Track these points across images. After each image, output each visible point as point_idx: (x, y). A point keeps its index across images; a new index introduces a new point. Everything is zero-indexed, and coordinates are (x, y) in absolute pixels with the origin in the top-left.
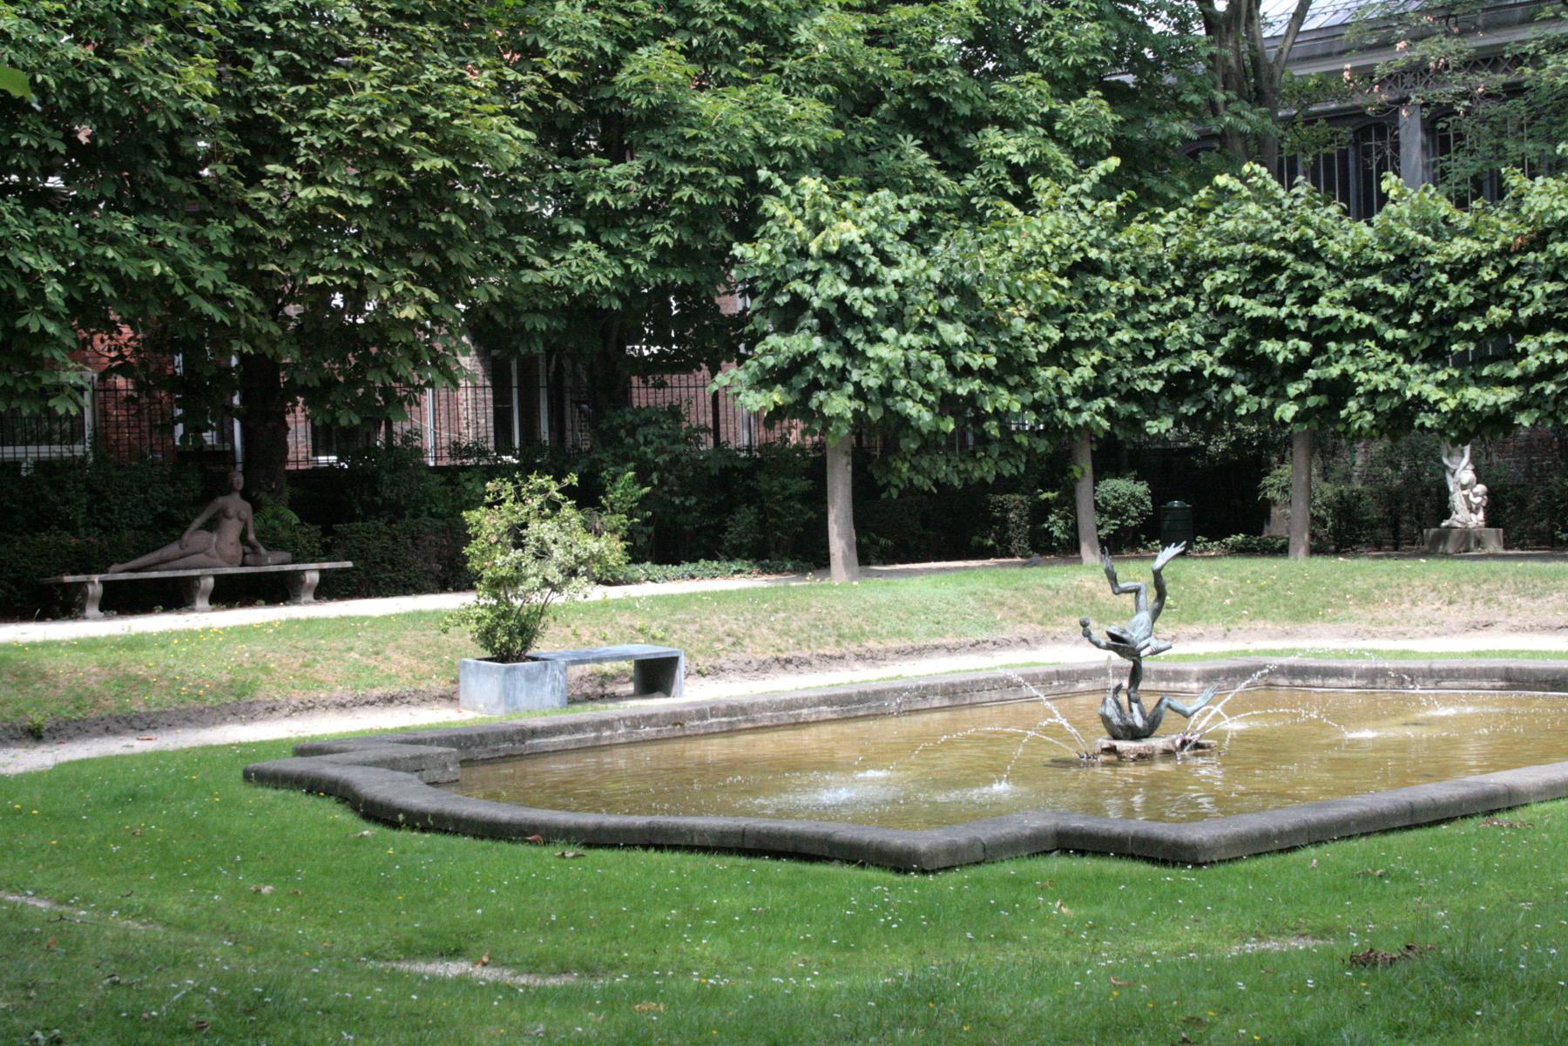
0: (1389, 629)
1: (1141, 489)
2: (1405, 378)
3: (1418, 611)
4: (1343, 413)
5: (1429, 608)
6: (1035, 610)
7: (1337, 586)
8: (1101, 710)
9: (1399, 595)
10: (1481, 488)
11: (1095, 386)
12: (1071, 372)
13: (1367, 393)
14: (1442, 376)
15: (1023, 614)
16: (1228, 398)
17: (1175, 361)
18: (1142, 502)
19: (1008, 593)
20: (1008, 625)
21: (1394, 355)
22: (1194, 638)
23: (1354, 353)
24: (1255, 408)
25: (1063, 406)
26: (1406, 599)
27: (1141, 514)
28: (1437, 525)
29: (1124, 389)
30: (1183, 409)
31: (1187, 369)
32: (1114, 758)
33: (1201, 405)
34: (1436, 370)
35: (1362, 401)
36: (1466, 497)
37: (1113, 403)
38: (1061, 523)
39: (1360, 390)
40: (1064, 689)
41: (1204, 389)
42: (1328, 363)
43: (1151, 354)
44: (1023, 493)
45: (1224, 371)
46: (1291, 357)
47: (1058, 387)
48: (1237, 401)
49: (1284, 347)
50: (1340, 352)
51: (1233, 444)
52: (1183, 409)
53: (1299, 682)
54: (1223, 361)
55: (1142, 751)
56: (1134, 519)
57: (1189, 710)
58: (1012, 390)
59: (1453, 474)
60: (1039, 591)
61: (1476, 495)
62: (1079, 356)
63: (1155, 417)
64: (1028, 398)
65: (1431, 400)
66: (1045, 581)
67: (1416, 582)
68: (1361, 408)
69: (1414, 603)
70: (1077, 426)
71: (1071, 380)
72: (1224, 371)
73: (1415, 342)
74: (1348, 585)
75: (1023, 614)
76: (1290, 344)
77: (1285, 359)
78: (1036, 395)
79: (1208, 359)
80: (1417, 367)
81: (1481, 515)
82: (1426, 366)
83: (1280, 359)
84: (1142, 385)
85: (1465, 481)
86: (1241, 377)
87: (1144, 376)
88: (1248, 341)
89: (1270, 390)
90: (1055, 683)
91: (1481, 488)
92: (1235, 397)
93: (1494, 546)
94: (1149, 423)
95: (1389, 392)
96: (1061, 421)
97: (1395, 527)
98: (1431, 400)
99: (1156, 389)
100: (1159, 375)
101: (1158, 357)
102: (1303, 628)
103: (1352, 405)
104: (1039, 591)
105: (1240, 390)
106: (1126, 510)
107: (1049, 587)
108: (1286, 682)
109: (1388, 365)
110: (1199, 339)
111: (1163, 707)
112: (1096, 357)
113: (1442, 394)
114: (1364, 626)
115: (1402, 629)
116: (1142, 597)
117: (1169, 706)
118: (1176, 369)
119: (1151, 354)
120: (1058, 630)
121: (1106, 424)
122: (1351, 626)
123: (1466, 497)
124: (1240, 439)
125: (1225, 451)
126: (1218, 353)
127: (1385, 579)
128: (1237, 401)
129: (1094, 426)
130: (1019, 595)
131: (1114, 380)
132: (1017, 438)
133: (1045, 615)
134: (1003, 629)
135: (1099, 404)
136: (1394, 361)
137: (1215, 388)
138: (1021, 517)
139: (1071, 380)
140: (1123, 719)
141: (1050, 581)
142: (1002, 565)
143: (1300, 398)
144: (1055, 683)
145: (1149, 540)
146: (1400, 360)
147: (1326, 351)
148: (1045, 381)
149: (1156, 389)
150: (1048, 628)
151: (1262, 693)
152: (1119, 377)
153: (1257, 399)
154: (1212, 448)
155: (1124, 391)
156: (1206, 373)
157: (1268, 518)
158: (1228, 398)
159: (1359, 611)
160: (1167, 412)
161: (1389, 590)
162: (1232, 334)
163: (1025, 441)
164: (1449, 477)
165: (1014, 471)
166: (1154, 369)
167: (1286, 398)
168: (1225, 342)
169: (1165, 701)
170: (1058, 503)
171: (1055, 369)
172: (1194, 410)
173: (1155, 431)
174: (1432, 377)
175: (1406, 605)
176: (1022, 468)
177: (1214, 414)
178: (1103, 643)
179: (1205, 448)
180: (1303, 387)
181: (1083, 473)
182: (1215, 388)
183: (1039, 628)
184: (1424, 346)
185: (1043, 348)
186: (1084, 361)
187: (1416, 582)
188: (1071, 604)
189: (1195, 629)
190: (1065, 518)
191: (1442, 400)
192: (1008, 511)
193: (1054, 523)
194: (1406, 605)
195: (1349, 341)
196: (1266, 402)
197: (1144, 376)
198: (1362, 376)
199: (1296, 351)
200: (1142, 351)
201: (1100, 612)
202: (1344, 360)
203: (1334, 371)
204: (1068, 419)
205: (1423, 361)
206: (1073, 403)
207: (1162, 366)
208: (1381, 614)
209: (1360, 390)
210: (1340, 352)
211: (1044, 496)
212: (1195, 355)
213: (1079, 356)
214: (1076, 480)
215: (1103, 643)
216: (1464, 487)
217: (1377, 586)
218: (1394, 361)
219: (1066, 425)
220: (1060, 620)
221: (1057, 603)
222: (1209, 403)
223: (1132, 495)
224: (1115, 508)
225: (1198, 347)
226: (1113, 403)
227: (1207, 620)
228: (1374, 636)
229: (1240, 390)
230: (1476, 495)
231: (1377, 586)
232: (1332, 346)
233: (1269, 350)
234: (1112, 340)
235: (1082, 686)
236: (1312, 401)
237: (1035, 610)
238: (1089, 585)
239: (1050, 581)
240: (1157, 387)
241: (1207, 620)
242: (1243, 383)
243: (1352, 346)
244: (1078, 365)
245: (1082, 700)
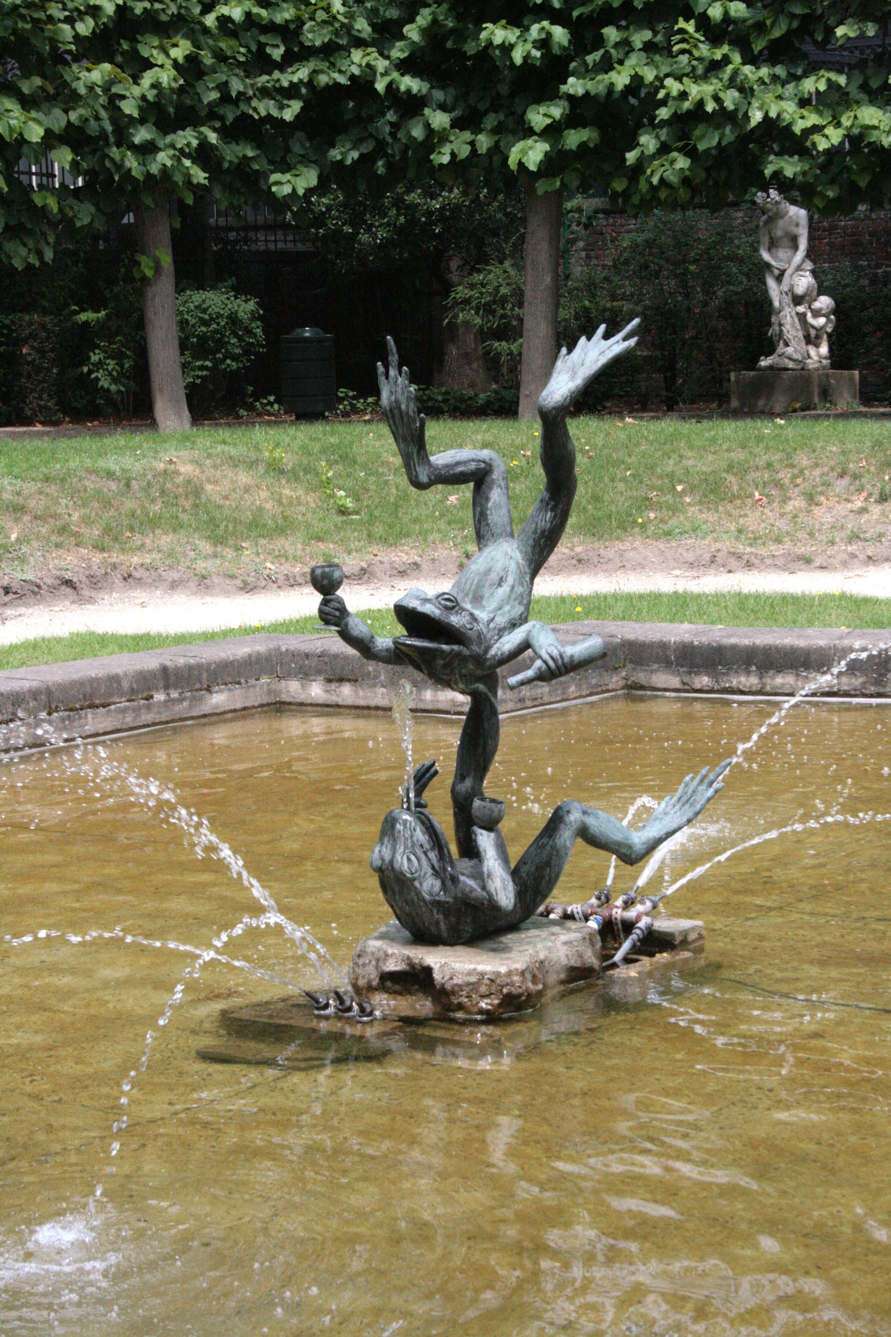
0: (778, 550)
1: (246, 307)
2: (746, 91)
3: (824, 515)
4: (631, 157)
5: (843, 509)
6: (86, 521)
7: (652, 468)
8: (380, 852)
9: (778, 484)
10: (824, 302)
11: (179, 107)
12: (136, 79)
13: (677, 119)
14: (811, 85)
15: (63, 530)
16: (418, 132)
17: (324, 65)
18: (249, 332)
19: (30, 487)
20: (33, 551)
21: (726, 49)
22: (402, 574)
23: (649, 47)
24: (464, 152)
25: (122, 139)
26: (793, 492)
27: (247, 352)
28: (752, 364)
29: (230, 114)
30: (335, 154)
31: (342, 80)
32: (423, 1006)
33: (368, 147)
34: (798, 79)
35: (664, 133)
36: (802, 317)
37: (213, 137)
38: (111, 364)
39: (663, 113)
40: (181, 709)
41: (371, 119)
42: (606, 65)
43: (277, 53)
44: (45, 312)
45: (410, 83)
46: (537, 54)
47: (114, 100)
48: (434, 139)
49: (522, 38)
50: (625, 45)
51: (400, 230)
52: (335, 154)
53: (705, 681)
54: (405, 66)
55: (518, 985)
56: (234, 358)
57: (639, 839)
58: (28, 103)
59: (779, 279)
60: (90, 484)
61: (816, 314)
62: (149, 48)
63: (286, 168)
64: (58, 119)
65: (797, 129)
66: (101, 463)
67: (803, 460)
68: (664, 149)
69: (810, 498)
70: (149, 176)
71: (136, 91)
72: (410, 83)
73: (760, 27)
74: (670, 465)
75: (63, 530)
76: (535, 31)
77: (526, 58)
78: (73, 116)
79: (381, 65)
80: (764, 72)
81: (824, 349)
82: (780, 70)
83: (518, 57)
84: (264, 107)
85: (800, 290)
86: (439, 95)
87: (265, 93)
88: (452, 31)
89: (490, 121)
90: (159, 697)
91: (824, 302)
92: (429, 130)
93: (846, 400)
94: (274, 177)
95: (723, 116)
96: (119, 167)
97: (669, 370)
98: (797, 129)
99: (288, 115)
100: (292, 92)
101: (290, 59)
102: (611, 550)
103: (648, 142)
104: (90, 484)
105: (439, 119)
106: (221, 344)
107: (110, 474)
108: (674, 681)
109: (715, 67)
110: (362, 26)
111: (566, 836)
112: (181, 50)
113: (813, 119)
114: (726, 545)
115: (802, 550)
116: (496, 496)
117: (585, 834)
118: (323, 79)
119: (277, 53)
120: (135, 560)
121: (200, 176)
122: (704, 546)
123: (802, 317)
124: (412, 222)
125: (387, 244)
126: (398, 52)
127: (739, 455)
128: (434, 139)
129: (178, 178)
130: (52, 489)
131: (214, 95)
132: (38, 200)
133: (107, 530)
134: (23, 560)
135: (187, 138)
136: (726, 60)
137: (391, 116)
138: (42, 352)
139: (136, 91)
140: (449, 880)
141: (111, 463)
142: (14, 436)
143: (552, 132)
144: (159, 697)
145: (257, 397)
146: (737, 58)
147: (599, 42)
148: (91, 88)
149: (288, 115)
150: (115, 557)
151: (620, 706)
152: (223, 87)
153: (467, 136)
154: (364, 238)
155: (230, 117)
156: (380, 86)
157: (441, 362)
158: (418, 132)
159: (712, 517)
160: (305, 160)
161: (753, 475)
162: (424, 18)
163: (52, 203)
164: (771, 283)
165: (33, 260)
166: (285, 79)
167: (529, 132)
168: (412, 32)
169: (574, 817)
170: (104, 330)
171: (107, 67)
172: (355, 155)
173: (287, 190)
174: (790, 88)
175: (797, 503)
176: (49, 255)
177: (389, 166)
178: (383, 642)
179: (353, 237)
180: (557, 111)
181: (158, 268)
182: (391, 116)
183: (97, 558)
184: (777, 34)
185: (85, 28)
186: (159, 58)
187: (803, 460)
188: (156, 508)
189: (403, 555)
190: (119, 357)
191: (817, 129)
192: (19, 342)
193: (100, 364)
194: (797, 503)
195: (640, 26)
196: (484, 142)
197: (265, 93)
198: (673, 86)
199: (544, 43)
200: (262, 46)
201: (212, 522)
202: (633, 60)
203: (620, 79)
204: (132, 162)
205: (773, 61)
206: (141, 135)
207: (301, 73)
208: (752, 520)
209: (663, 113)
210: (625, 45)
211: (83, 317)
212: (357, 55)
213: (149, 48)
214: (144, 280)
215: (383, 642)
216: (797, 300)
217: (730, 469)
218: (726, 60)
219: (127, 175)
220: (138, 540)
221: (129, 504)
222: (380, 147)
223: (233, 319)
224: (203, 338)
225: (360, 43)
226: (213, 137)
227: (424, 534)
228: (749, 565)
229: (439, 119)
230: (816, 314)
231: (730, 469)
232: (611, 34)
233: (498, 40)
234: (210, 20)
235: (219, 699)
236: (573, 139)
237: (86, 521)
238: (186, 469)
239: (111, 463)
240: (291, 111)
241: (424, 534)
242: (443, 107)
243: (647, 35)
244: (148, 65)
245: (220, 735)
